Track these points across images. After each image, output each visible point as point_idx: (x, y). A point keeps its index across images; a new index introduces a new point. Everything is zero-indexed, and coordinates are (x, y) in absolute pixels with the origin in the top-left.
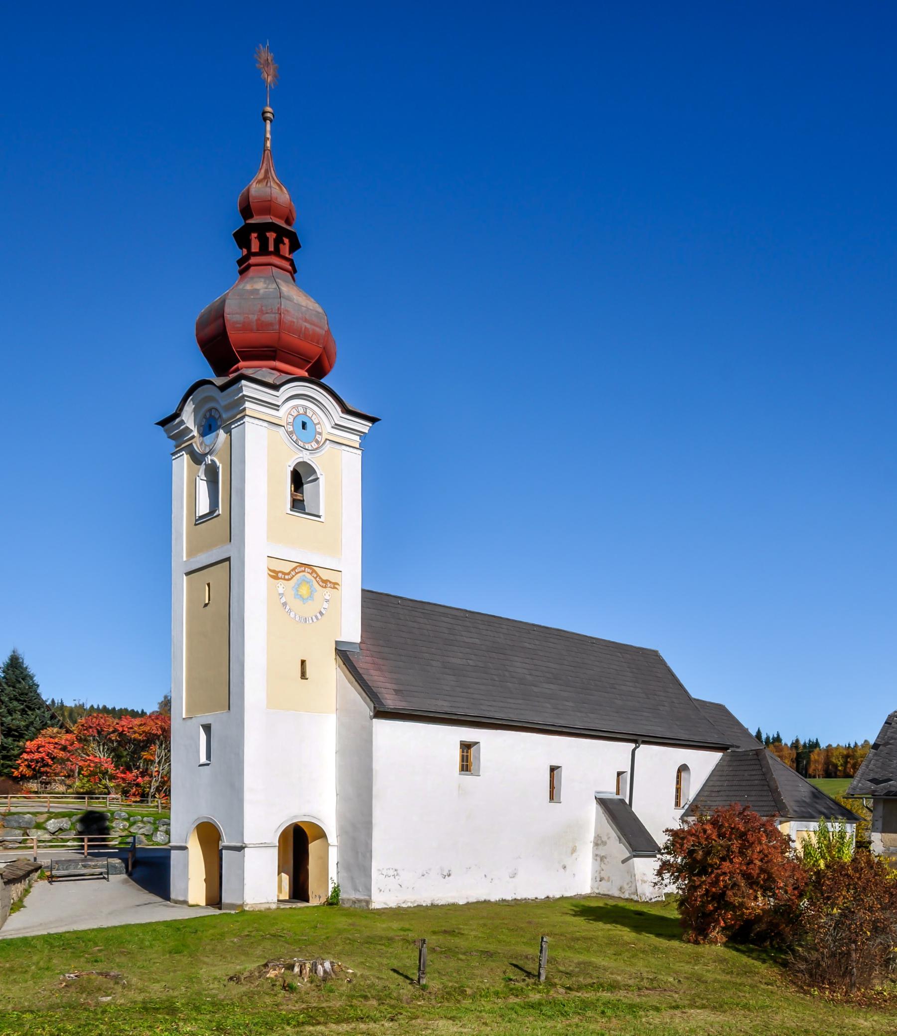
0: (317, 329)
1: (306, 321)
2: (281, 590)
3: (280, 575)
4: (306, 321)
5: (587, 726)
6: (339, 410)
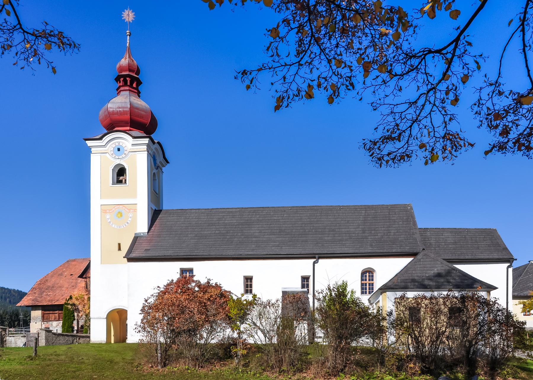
0: (125, 109)
1: (119, 108)
2: (108, 217)
3: (107, 211)
4: (119, 108)
5: (274, 253)
6: (131, 138)
